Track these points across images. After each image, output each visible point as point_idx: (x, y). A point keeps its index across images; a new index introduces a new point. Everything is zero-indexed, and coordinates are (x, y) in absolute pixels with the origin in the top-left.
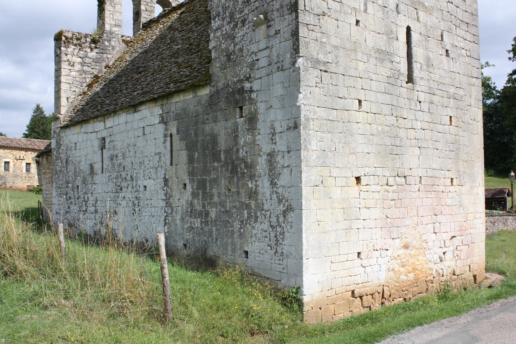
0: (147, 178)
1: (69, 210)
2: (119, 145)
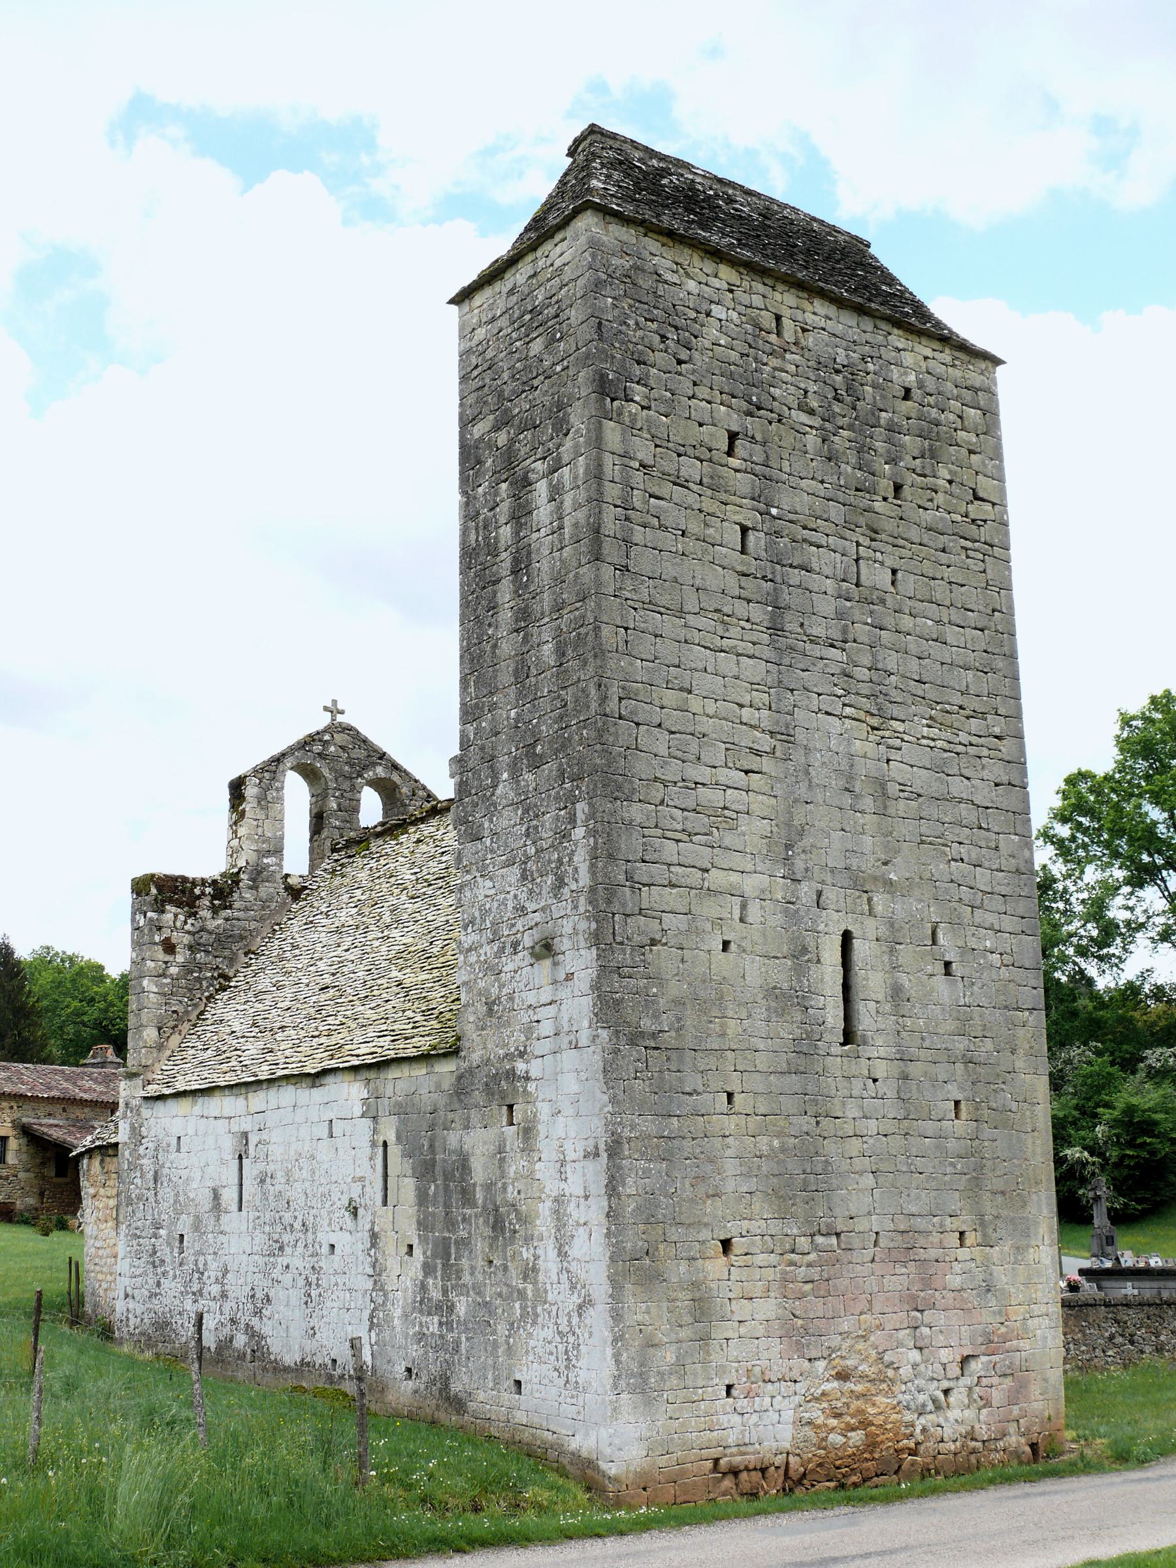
0: (337, 1229)
1: (158, 1291)
2: (276, 1151)
